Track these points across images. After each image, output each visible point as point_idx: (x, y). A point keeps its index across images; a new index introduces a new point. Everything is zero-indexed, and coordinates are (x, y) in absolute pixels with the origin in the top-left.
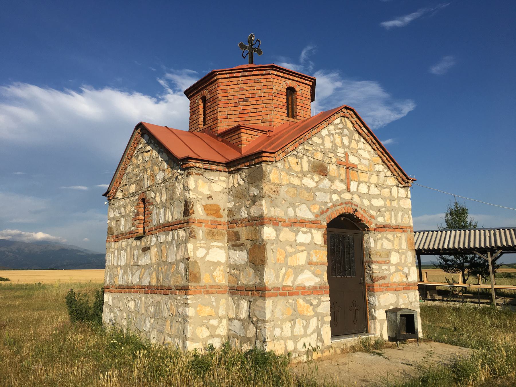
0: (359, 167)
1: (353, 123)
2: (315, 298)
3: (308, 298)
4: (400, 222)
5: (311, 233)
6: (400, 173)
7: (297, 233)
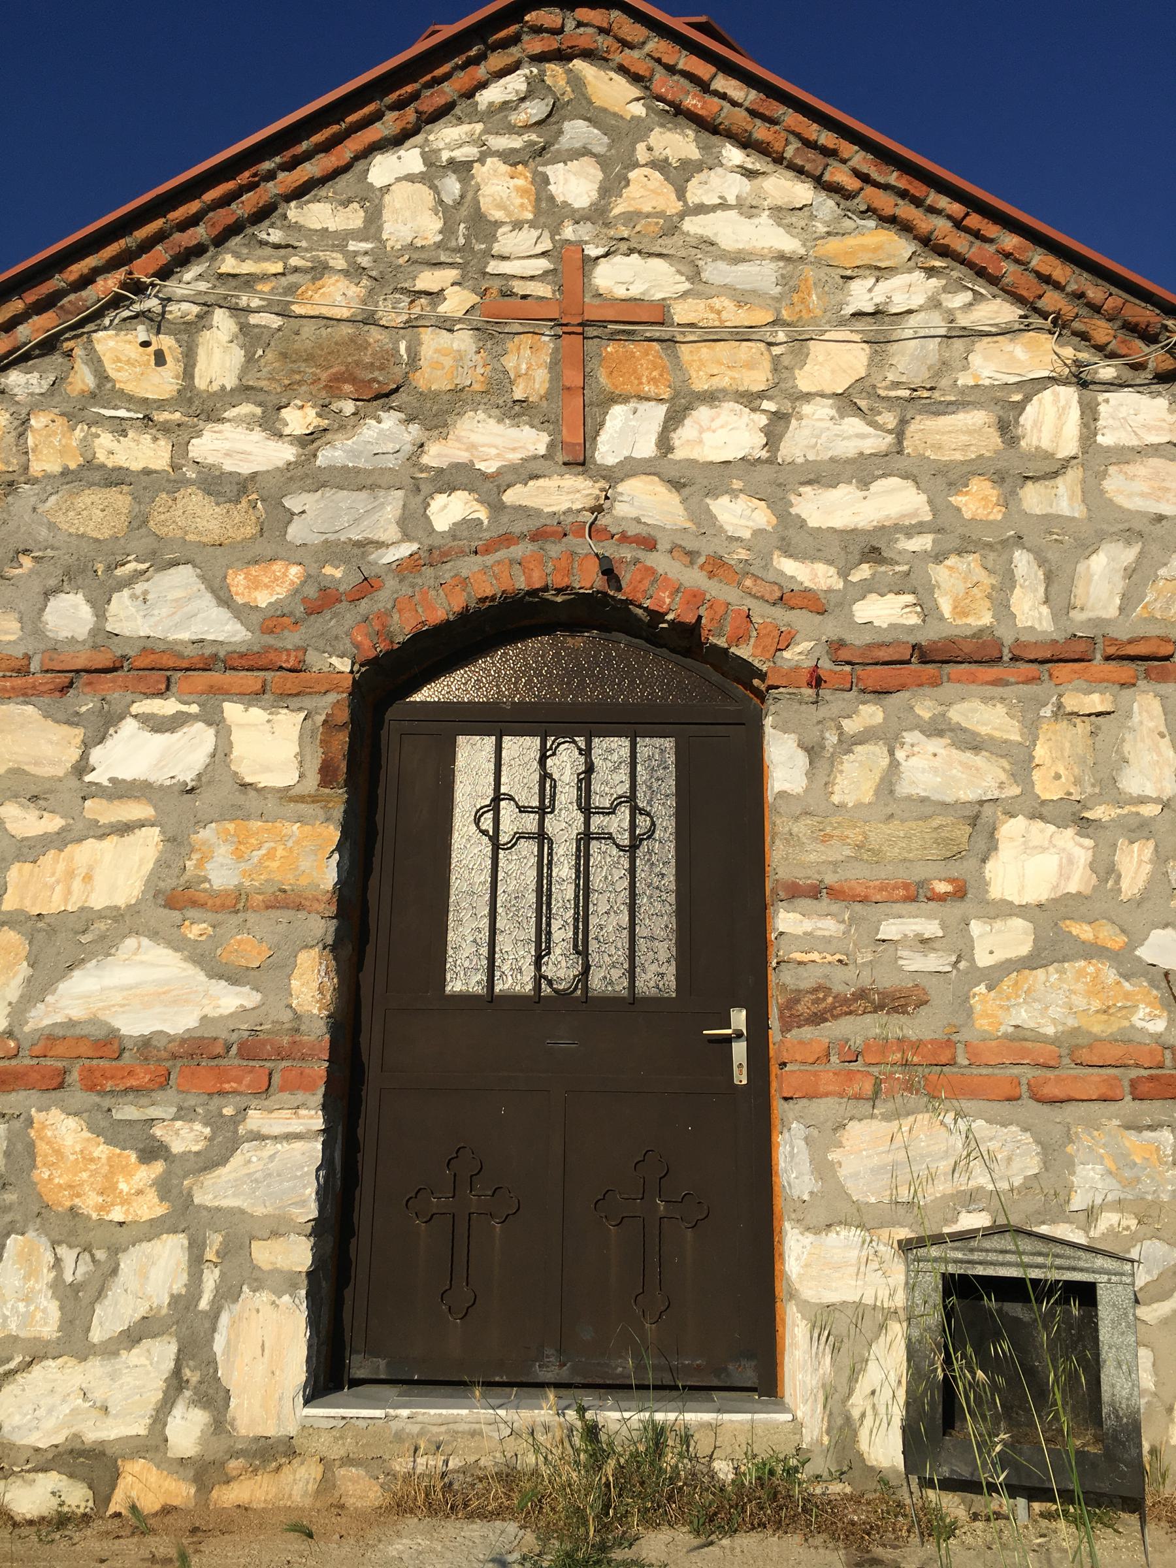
0: (682, 313)
1: (636, 78)
2: (184, 1114)
3: (128, 1111)
4: (1112, 612)
5: (214, 719)
6: (1095, 292)
7: (101, 728)
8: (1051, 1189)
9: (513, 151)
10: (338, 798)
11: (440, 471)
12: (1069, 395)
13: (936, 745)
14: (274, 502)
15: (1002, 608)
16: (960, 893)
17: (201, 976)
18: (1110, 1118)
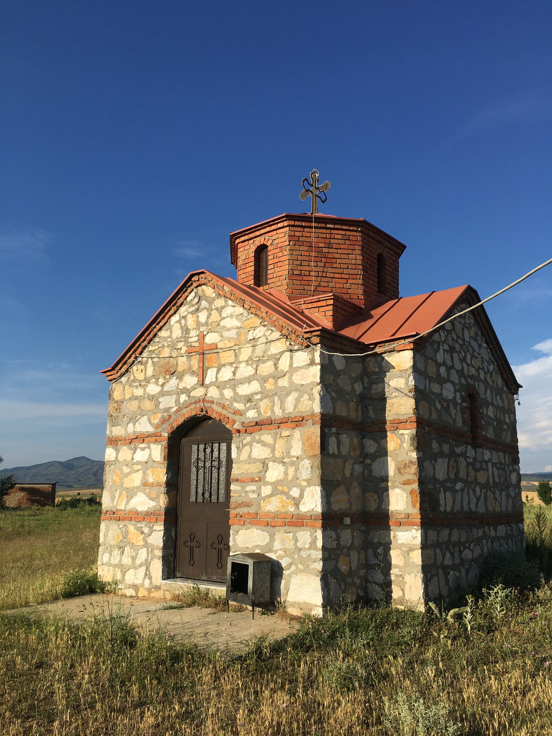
4: (292, 410)
8: (269, 547)
9: (193, 311)
10: (166, 463)
11: (181, 389)
12: (288, 354)
13: (259, 445)
14: (157, 400)
15: (273, 412)
16: (260, 480)
17: (148, 499)
18: (282, 529)
